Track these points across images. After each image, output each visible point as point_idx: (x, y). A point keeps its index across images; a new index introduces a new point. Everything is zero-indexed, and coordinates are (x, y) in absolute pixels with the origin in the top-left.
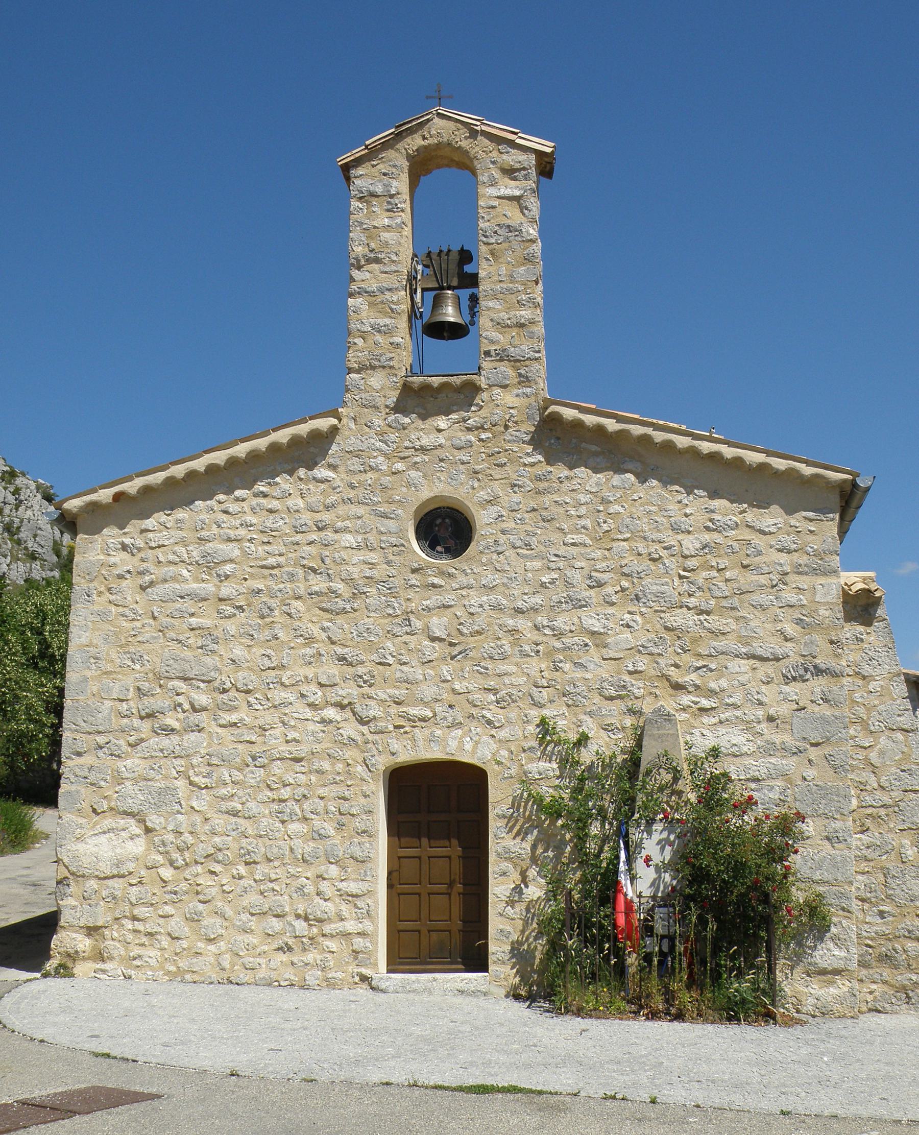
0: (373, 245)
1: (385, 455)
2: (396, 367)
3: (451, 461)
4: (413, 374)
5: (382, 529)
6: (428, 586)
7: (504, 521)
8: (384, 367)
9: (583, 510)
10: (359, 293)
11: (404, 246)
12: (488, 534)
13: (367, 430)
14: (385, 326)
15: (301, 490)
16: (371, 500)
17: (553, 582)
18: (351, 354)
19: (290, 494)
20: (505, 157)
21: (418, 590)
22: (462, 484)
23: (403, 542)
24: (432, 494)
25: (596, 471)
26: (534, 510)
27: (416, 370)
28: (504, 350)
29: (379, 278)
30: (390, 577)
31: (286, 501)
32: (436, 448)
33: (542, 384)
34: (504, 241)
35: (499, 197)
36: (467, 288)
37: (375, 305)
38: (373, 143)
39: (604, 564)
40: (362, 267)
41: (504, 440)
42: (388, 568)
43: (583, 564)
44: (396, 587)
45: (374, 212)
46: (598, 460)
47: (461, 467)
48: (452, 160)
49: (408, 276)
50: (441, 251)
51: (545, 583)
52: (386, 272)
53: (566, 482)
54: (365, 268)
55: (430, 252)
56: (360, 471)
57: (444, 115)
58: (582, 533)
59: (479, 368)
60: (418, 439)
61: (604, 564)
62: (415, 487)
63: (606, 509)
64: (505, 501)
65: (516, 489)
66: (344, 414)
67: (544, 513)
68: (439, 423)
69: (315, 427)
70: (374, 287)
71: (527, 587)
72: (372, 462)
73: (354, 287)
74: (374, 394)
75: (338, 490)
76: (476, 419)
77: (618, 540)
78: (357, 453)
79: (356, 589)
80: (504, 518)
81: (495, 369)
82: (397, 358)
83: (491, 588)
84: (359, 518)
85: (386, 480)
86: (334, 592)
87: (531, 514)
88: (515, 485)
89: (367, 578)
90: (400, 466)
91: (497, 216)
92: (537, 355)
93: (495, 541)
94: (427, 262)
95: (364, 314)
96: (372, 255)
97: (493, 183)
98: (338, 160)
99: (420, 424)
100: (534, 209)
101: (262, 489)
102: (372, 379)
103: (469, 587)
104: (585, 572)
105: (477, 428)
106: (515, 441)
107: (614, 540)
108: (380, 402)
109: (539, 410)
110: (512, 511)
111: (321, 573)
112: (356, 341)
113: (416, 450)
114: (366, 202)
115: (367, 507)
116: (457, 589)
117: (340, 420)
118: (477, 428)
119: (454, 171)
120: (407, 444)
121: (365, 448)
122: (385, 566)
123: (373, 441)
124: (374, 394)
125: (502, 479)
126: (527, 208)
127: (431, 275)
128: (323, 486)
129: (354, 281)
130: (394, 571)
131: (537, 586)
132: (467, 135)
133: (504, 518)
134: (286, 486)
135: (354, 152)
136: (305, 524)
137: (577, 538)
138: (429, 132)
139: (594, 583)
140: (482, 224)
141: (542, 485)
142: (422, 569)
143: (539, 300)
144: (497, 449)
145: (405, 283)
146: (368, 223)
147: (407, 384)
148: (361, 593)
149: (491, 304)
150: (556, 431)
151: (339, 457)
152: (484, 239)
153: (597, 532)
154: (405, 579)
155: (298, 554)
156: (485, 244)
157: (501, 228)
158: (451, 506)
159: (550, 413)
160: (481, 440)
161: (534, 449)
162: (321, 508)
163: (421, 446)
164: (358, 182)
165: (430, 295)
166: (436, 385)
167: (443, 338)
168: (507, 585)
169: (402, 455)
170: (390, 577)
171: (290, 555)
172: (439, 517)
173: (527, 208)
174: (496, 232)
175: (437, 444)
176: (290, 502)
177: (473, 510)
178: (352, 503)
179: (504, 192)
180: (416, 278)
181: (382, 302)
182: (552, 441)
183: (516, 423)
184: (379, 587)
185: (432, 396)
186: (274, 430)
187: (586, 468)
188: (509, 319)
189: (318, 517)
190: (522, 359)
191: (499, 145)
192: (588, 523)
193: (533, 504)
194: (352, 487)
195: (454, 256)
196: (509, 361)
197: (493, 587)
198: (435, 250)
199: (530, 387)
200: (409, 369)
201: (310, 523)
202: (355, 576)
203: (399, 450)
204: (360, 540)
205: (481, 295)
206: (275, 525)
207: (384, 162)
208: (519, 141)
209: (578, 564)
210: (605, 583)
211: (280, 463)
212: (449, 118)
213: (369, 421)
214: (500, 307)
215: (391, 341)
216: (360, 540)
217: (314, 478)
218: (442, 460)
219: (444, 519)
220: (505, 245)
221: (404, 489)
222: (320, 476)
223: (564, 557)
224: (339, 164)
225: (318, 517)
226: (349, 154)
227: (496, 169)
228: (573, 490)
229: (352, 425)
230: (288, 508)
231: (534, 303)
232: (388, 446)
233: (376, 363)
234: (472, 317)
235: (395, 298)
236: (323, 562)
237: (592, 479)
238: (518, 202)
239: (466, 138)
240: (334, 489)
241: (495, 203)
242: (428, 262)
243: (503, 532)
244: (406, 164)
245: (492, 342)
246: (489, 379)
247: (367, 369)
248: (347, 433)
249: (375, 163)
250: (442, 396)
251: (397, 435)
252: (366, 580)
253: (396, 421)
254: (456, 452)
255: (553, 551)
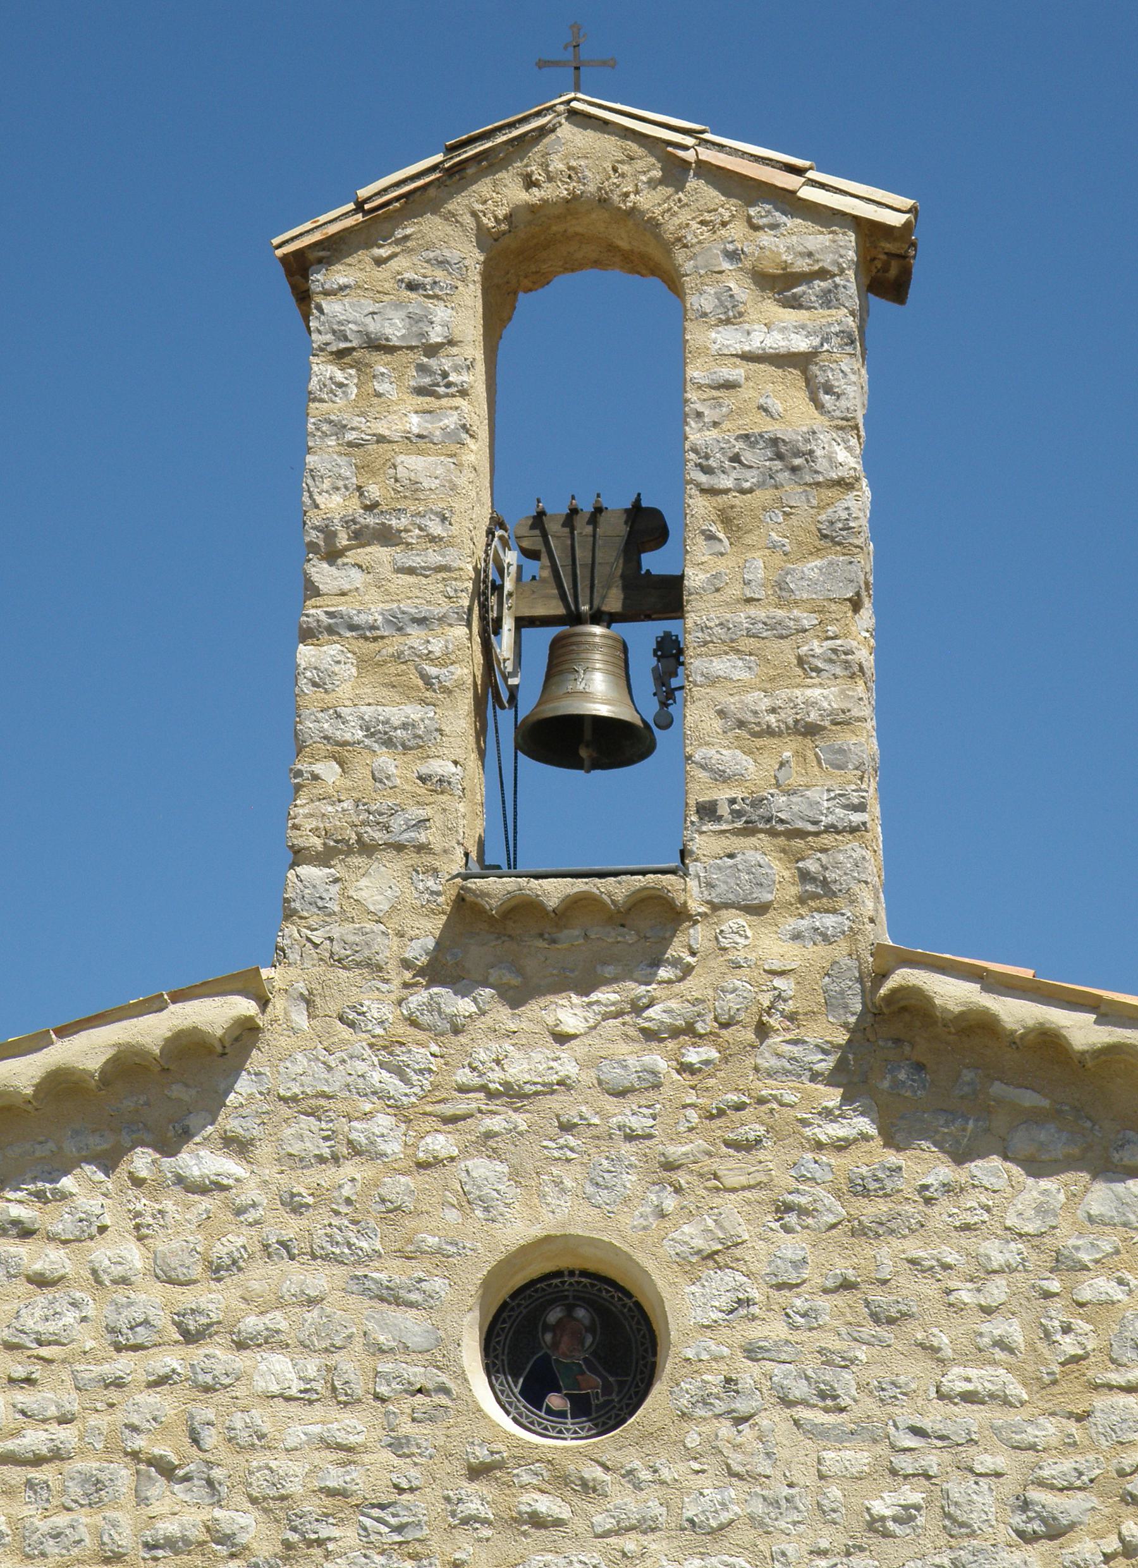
0: (374, 491)
1: (398, 1110)
2: (437, 848)
3: (595, 1132)
4: (488, 869)
5: (382, 1339)
6: (518, 1520)
7: (754, 1318)
8: (399, 848)
9: (997, 1290)
10: (331, 630)
11: (466, 496)
12: (705, 1357)
13: (345, 1032)
14: (404, 726)
15: (138, 1214)
16: (349, 1245)
17: (906, 1516)
18: (302, 808)
19: (103, 1229)
20: (766, 239)
21: (486, 1532)
22: (627, 1200)
23: (444, 1378)
24: (536, 1232)
25: (1036, 1168)
26: (847, 1285)
27: (496, 855)
28: (758, 802)
29: (392, 588)
30: (401, 1491)
31: (90, 1251)
32: (549, 1090)
33: (870, 903)
34: (761, 485)
35: (747, 357)
36: (648, 618)
37: (378, 665)
38: (379, 194)
39: (1067, 1465)
40: (341, 553)
41: (756, 1069)
42: (397, 1462)
43: (998, 1461)
44: (419, 1524)
45: (378, 395)
46: (1043, 1136)
47: (627, 1148)
48: (612, 248)
49: (476, 581)
50: (574, 511)
51: (883, 1519)
52: (411, 571)
53: (944, 1201)
54: (351, 557)
55: (541, 514)
56: (321, 1159)
57: (590, 116)
58: (994, 1363)
59: (683, 854)
60: (498, 1062)
61: (1067, 1465)
62: (486, 1210)
63: (1070, 1290)
64: (757, 1255)
65: (791, 1219)
66: (278, 984)
67: (878, 1297)
68: (562, 1015)
69: (186, 1024)
70: (374, 611)
71: (826, 1530)
72: (358, 1132)
73: (315, 612)
74: (369, 926)
75: (251, 1216)
76: (673, 1004)
77: (1110, 1387)
78: (313, 1102)
79: (294, 1529)
80: (755, 1310)
81: (731, 856)
82: (438, 820)
83: (712, 1532)
84: (312, 1302)
85: (399, 1186)
86: (224, 1539)
87: (840, 1300)
88: (789, 1208)
89: (331, 1493)
90: (441, 1143)
91: (740, 412)
92: (856, 818)
93: (728, 1380)
94: (533, 542)
95: (344, 691)
96: (371, 520)
97: (731, 316)
98: (276, 241)
99: (502, 1015)
100: (851, 390)
101: (16, 1211)
102: (364, 882)
103: (644, 1526)
104: (1009, 1487)
105: (676, 1033)
106: (787, 1073)
107: (1097, 1387)
108: (387, 949)
109: (860, 980)
110: (780, 1287)
111: (187, 1478)
112: (319, 768)
113: (491, 1095)
114: (357, 365)
115: (339, 1271)
116: (606, 1534)
117: (264, 1003)
118: (676, 1033)
119: (616, 278)
120: (464, 1076)
121: (336, 1086)
122: (387, 1456)
123: (361, 1067)
124: (369, 926)
125: (750, 1187)
126: (829, 390)
127: (544, 580)
128: (205, 1203)
129: (317, 593)
130: (413, 1472)
131: (858, 1525)
132: (657, 174)
133: (755, 1310)
134: (89, 1203)
135: (323, 219)
136: (146, 1323)
137: (981, 1378)
138: (545, 166)
139: (1036, 1526)
140: (696, 435)
141: (872, 1210)
142: (500, 1465)
143: (864, 656)
144: (733, 1097)
145: (466, 603)
146: (362, 427)
147: (469, 897)
148: (310, 1544)
149: (720, 666)
150: (913, 1045)
151: (258, 1114)
152: (703, 478)
153: (1041, 1359)
154: (447, 1499)
155: (119, 1417)
156: (703, 491)
157: (753, 445)
158: (592, 1267)
159: (894, 992)
160: (685, 1068)
161: (846, 1099)
162: (197, 1271)
163: (507, 1085)
164: (332, 307)
165: (540, 639)
166: (552, 903)
167: (575, 763)
168: (762, 1524)
169: (447, 1109)
170: (401, 1491)
171: (93, 1420)
172: (551, 1303)
173: (829, 390)
174: (736, 459)
175: (555, 1078)
176: (102, 1253)
177: (661, 1284)
178: (292, 1258)
179: (761, 340)
180: (498, 588)
181: (398, 657)
182: (902, 1076)
183: (792, 1017)
184: (368, 1522)
185: (541, 935)
186: (64, 1032)
187: (1006, 1158)
188: (773, 711)
189: (186, 1298)
190: (811, 828)
191: (751, 203)
192: (1014, 1330)
193: (843, 1267)
194: (293, 1204)
195: (614, 527)
196: (773, 833)
197: (721, 1527)
198: (557, 508)
199: (834, 911)
200: (474, 855)
201: (162, 1320)
202: (294, 1488)
203: (440, 1094)
204: (311, 1371)
205: (690, 641)
206: (52, 1327)
207: (410, 251)
208: (808, 193)
209: (986, 1462)
210: (1072, 1526)
211: (76, 1133)
212: (604, 125)
213: (353, 1008)
214: (745, 675)
215: (424, 770)
216: (311, 1371)
217: (180, 1180)
218: (567, 1127)
219: (570, 1309)
220: (763, 496)
221: (452, 1215)
222: (196, 1172)
223: (941, 1438)
224: (279, 252)
225: (186, 1298)
226: (308, 225)
227: (739, 276)
228: (966, 1227)
229: (300, 1018)
230: (94, 1272)
231: (847, 665)
232: (406, 1081)
233: (377, 835)
234: (664, 704)
235: (437, 647)
236: (196, 1441)
237: (1025, 1196)
238: (804, 372)
239: (653, 184)
240: (239, 1212)
241: (736, 372)
242: (537, 544)
243: (752, 1352)
244: (473, 258)
245: (722, 777)
246: (710, 885)
247: (349, 852)
248: (283, 1042)
249: (383, 252)
250: (571, 934)
251: (435, 1049)
252: (328, 1501)
253: (434, 1006)
254: (610, 1104)
255: (906, 1416)
